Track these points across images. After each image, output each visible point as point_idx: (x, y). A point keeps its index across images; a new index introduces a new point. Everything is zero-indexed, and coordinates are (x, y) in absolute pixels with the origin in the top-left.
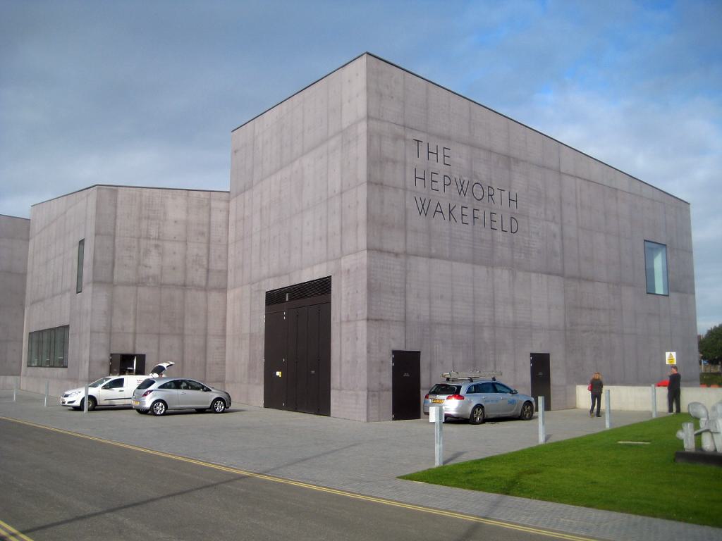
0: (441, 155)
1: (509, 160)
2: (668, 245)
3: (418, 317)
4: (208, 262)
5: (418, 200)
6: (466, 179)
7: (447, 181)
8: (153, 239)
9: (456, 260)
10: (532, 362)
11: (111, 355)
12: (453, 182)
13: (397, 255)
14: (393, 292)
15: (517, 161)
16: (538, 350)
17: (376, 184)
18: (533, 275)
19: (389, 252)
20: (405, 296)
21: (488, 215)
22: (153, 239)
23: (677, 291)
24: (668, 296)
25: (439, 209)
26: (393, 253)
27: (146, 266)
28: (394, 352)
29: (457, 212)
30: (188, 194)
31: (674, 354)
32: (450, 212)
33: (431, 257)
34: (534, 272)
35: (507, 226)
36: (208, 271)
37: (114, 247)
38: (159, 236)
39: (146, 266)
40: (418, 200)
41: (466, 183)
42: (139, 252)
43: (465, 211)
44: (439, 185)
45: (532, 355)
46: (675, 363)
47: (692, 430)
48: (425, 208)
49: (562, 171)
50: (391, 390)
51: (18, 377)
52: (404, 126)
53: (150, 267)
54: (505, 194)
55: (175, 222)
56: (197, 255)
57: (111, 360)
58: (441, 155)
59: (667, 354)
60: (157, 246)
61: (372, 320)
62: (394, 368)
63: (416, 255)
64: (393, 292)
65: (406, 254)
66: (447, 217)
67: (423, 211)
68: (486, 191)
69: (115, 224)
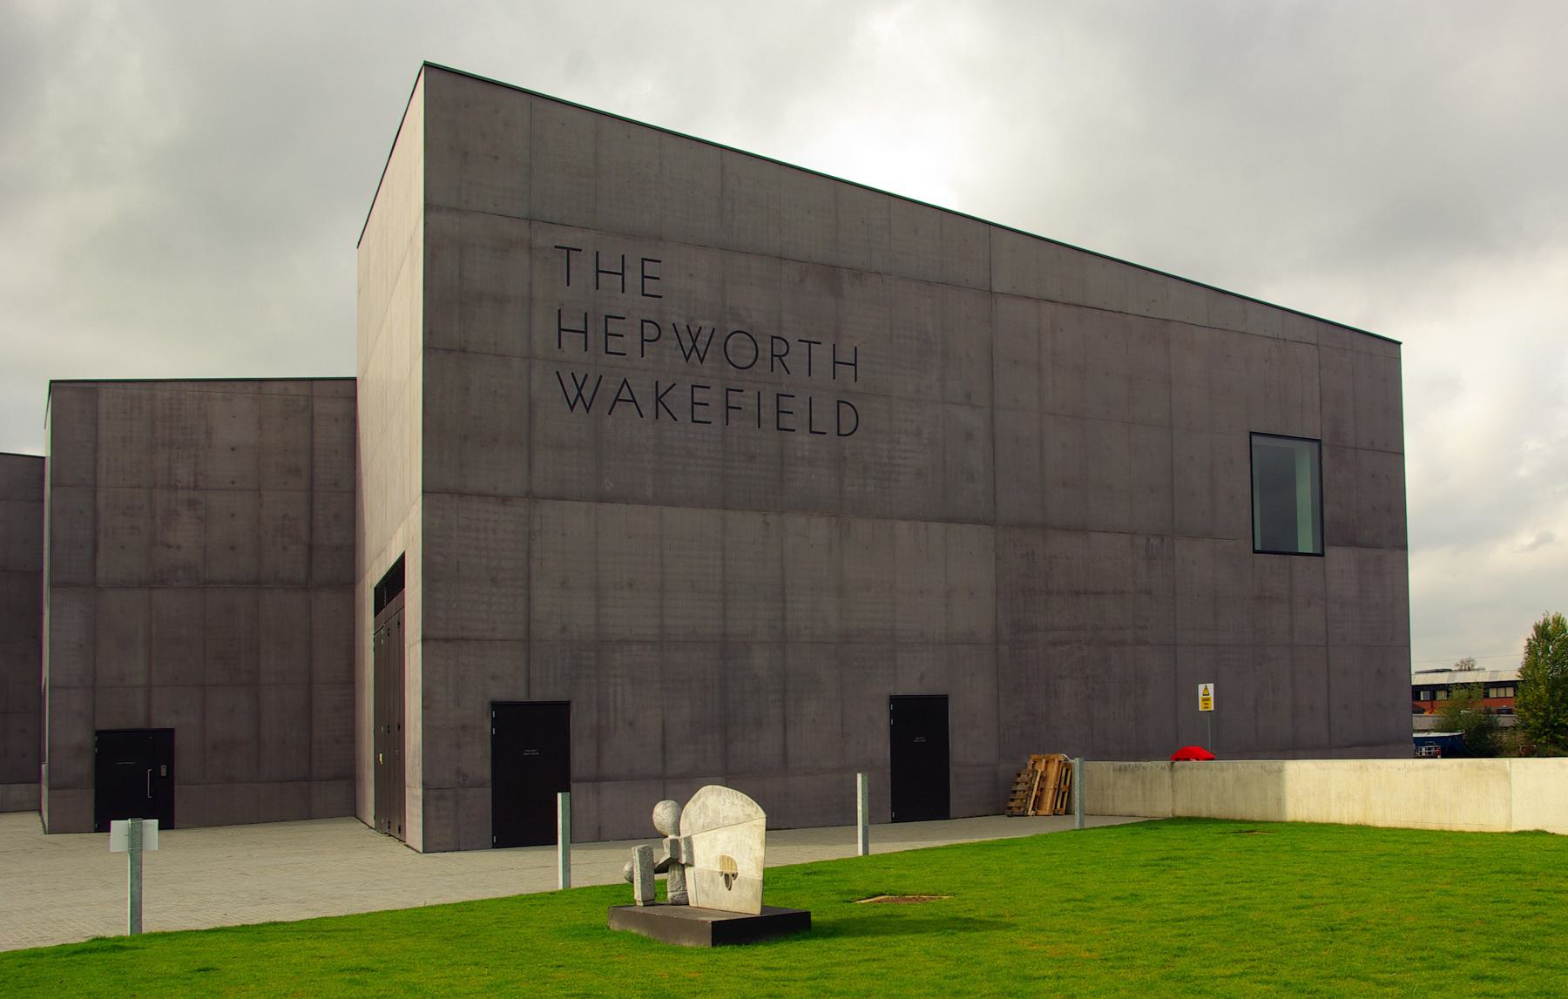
0: (633, 277)
1: (832, 274)
2: (1325, 441)
3: (564, 629)
4: (311, 530)
5: (568, 381)
6: (707, 325)
7: (651, 331)
8: (183, 488)
9: (672, 504)
10: (893, 714)
11: (98, 733)
12: (668, 332)
13: (504, 499)
14: (493, 580)
15: (858, 274)
16: (910, 686)
17: (449, 351)
18: (902, 526)
19: (482, 495)
20: (528, 588)
21: (768, 402)
22: (183, 488)
23: (1352, 543)
24: (1322, 555)
25: (625, 394)
26: (495, 496)
27: (170, 547)
28: (496, 706)
29: (679, 399)
30: (260, 388)
31: (1211, 687)
32: (658, 399)
33: (601, 499)
34: (905, 519)
35: (825, 419)
36: (311, 548)
37: (95, 510)
38: (196, 481)
39: (170, 547)
40: (568, 381)
41: (706, 332)
42: (153, 518)
43: (700, 395)
44: (631, 341)
45: (894, 700)
46: (1213, 709)
47: (387, 848)
48: (587, 394)
49: (996, 288)
50: (490, 784)
51: (33, 786)
52: (530, 220)
53: (179, 548)
54: (822, 354)
55: (233, 449)
56: (285, 516)
57: (97, 744)
58: (633, 277)
59: (1201, 687)
60: (192, 504)
61: (436, 639)
62: (495, 740)
63: (559, 497)
64: (493, 580)
65: (532, 497)
66: (648, 410)
67: (580, 397)
68: (765, 348)
69: (96, 461)
